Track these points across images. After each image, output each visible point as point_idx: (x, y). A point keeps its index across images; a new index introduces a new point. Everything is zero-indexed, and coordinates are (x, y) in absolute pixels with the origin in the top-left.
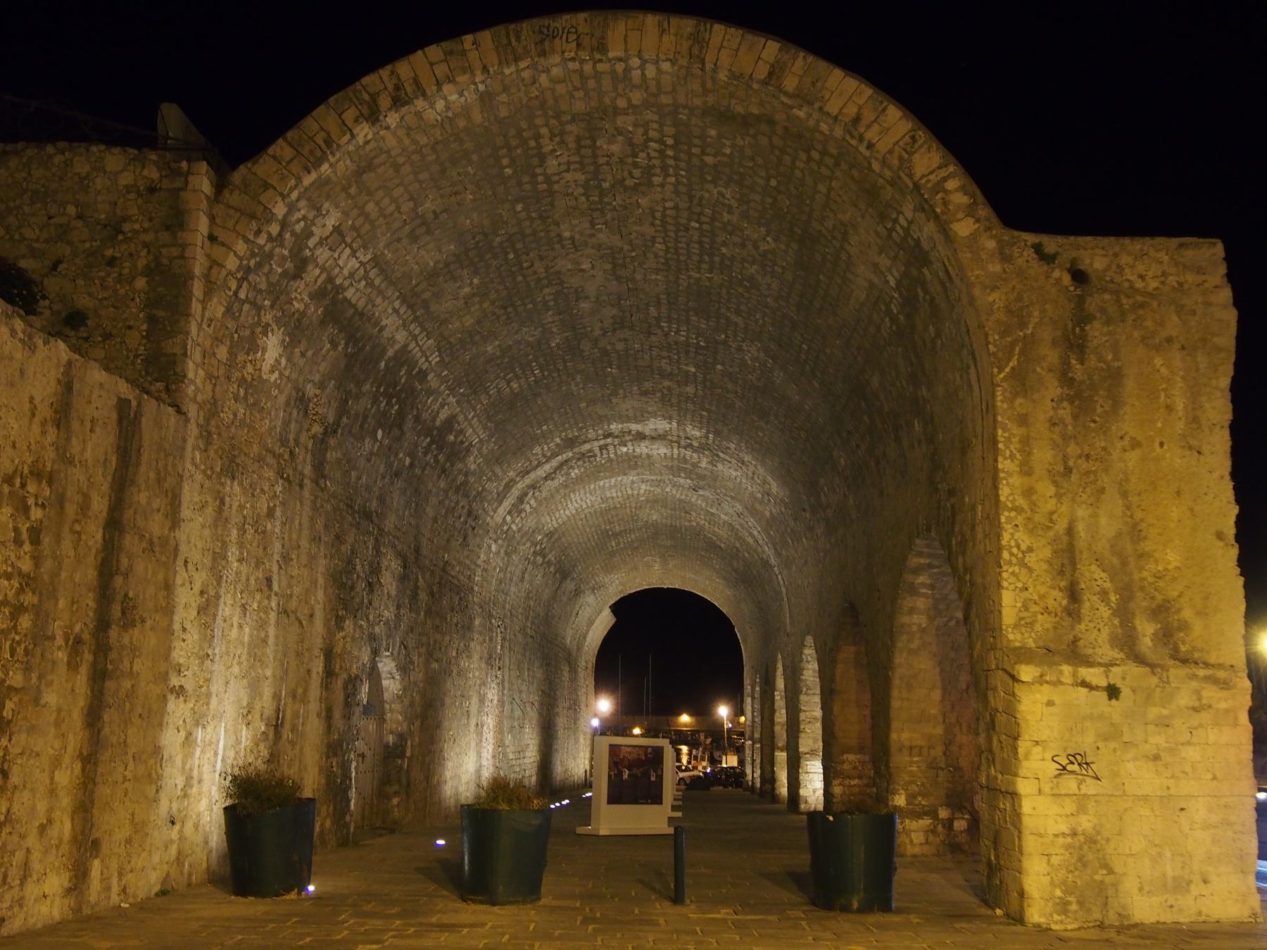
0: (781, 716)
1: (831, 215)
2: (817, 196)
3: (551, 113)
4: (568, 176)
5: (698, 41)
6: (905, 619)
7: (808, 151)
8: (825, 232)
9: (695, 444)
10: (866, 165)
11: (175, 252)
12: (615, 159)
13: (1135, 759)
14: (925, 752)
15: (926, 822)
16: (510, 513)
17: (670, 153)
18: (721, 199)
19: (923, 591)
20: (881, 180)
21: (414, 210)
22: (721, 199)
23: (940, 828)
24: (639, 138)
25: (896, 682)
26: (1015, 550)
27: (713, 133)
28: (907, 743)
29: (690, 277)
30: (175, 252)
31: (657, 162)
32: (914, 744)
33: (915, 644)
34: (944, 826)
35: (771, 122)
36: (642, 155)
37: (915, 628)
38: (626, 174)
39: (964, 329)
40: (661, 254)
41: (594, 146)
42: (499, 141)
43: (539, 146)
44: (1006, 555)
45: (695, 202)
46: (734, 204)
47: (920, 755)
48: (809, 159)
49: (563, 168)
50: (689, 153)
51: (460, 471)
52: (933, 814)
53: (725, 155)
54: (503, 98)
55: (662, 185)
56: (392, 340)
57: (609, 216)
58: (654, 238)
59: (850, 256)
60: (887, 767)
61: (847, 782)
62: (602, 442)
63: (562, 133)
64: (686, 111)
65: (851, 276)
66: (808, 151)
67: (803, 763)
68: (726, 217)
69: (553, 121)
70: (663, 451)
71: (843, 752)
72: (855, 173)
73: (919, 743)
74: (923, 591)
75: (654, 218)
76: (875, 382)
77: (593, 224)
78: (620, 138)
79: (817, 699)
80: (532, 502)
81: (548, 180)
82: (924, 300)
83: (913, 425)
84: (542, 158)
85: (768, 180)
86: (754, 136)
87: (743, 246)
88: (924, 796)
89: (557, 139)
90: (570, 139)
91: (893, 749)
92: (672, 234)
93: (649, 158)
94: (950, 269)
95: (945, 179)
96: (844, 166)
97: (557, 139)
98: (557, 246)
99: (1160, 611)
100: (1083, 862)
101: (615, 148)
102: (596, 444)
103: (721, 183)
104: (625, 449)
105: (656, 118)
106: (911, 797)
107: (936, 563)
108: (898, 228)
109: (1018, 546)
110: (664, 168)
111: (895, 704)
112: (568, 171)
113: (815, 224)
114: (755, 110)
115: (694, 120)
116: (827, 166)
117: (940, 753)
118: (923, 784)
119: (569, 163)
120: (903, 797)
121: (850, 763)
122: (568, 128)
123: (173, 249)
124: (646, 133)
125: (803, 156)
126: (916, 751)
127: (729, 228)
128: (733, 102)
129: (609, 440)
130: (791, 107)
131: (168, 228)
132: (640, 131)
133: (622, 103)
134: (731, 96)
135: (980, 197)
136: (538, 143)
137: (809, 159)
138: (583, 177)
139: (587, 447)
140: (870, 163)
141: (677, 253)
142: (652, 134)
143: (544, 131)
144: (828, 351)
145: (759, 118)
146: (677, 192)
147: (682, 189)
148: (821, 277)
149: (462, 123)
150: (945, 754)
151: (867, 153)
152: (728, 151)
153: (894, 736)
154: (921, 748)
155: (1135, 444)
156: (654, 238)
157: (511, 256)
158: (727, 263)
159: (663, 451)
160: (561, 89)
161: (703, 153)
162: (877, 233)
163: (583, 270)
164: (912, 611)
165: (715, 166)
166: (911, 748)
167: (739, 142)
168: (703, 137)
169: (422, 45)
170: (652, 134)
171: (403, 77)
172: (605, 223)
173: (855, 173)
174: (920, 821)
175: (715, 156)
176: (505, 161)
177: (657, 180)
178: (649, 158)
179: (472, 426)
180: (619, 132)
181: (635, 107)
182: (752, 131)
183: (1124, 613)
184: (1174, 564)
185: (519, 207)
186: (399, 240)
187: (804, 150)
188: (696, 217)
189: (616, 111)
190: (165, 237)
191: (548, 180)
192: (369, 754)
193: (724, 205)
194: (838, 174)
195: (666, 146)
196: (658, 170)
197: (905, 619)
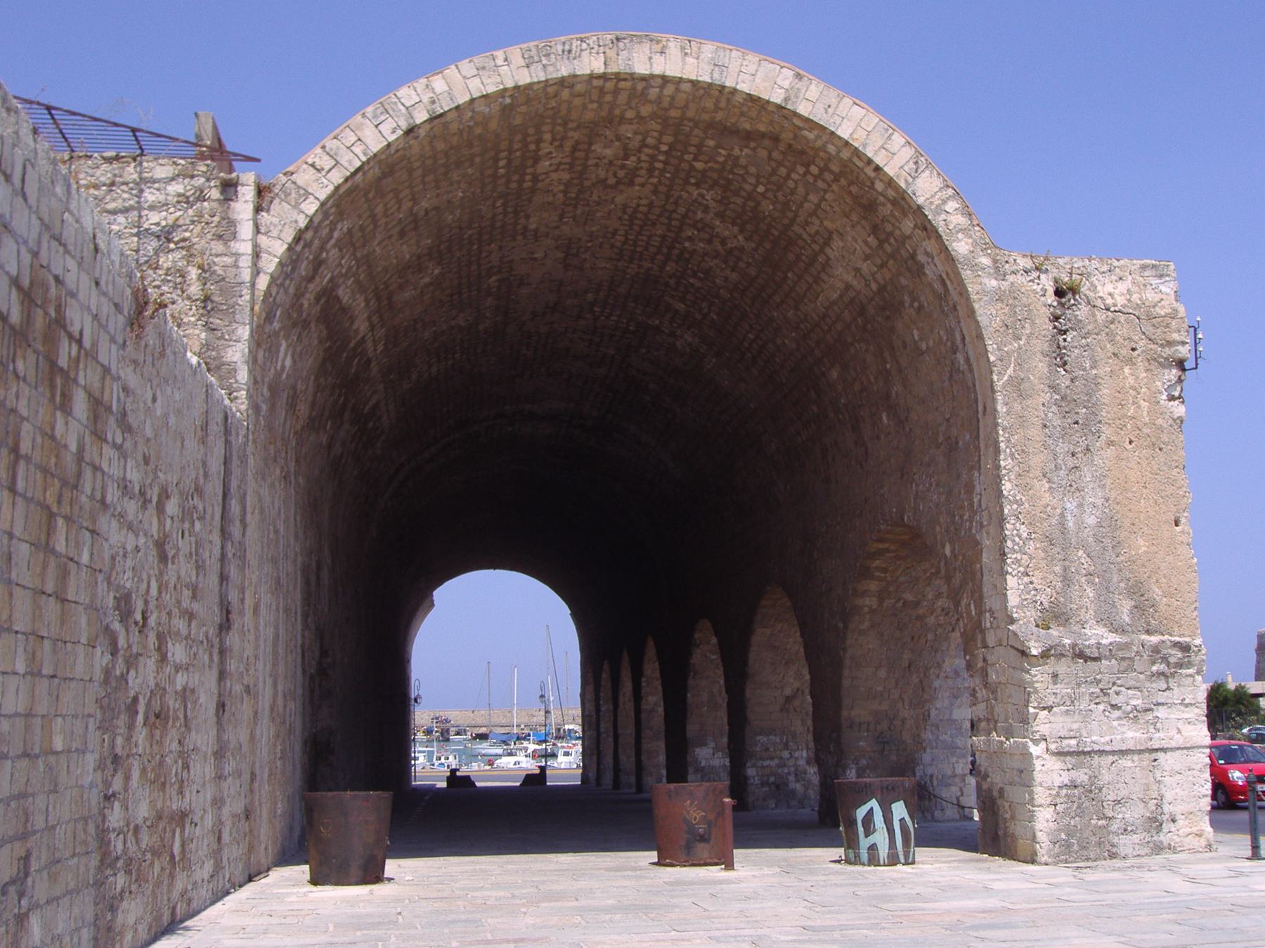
0: (605, 725)
1: (817, 222)
2: (806, 205)
3: (559, 121)
4: (554, 176)
5: (786, 99)
6: (859, 602)
7: (807, 165)
8: (805, 236)
10: (868, 184)
11: (228, 260)
12: (606, 161)
13: (1119, 718)
17: (661, 158)
18: (700, 199)
19: (877, 574)
20: (881, 198)
21: (411, 209)
22: (700, 199)
24: (635, 143)
25: (847, 662)
26: (1017, 539)
27: (711, 143)
29: (640, 267)
30: (228, 260)
31: (644, 165)
33: (866, 625)
35: (776, 139)
36: (633, 158)
37: (866, 609)
38: (610, 174)
39: (958, 337)
40: (618, 244)
41: (588, 151)
42: (504, 145)
43: (538, 149)
44: (1009, 543)
45: (671, 200)
46: (712, 204)
47: (868, 730)
48: (807, 172)
49: (553, 168)
50: (681, 159)
53: (717, 162)
54: (523, 109)
55: (642, 185)
56: (357, 331)
57: (579, 212)
58: (616, 230)
59: (829, 259)
61: (760, 763)
63: (564, 138)
64: (691, 124)
65: (825, 277)
66: (807, 165)
68: (700, 215)
69: (558, 128)
71: (760, 734)
72: (854, 189)
74: (877, 574)
75: (624, 212)
76: (834, 374)
77: (561, 217)
78: (617, 143)
81: (535, 178)
82: (911, 306)
83: (881, 419)
84: (536, 160)
85: (756, 186)
86: (754, 149)
87: (710, 241)
89: (557, 143)
90: (568, 145)
92: (637, 228)
93: (639, 160)
94: (948, 283)
95: (944, 202)
96: (843, 182)
97: (557, 143)
98: (520, 237)
99: (1136, 591)
100: (1081, 812)
101: (608, 152)
103: (706, 186)
105: (659, 127)
107: (893, 547)
108: (892, 240)
109: (1020, 537)
110: (651, 171)
111: (846, 683)
112: (556, 171)
113: (796, 228)
114: (762, 128)
115: (696, 131)
116: (824, 181)
119: (560, 163)
122: (571, 134)
123: (225, 259)
124: (643, 140)
125: (801, 170)
127: (700, 225)
128: (743, 119)
130: (800, 128)
131: (220, 237)
132: (639, 137)
133: (630, 114)
134: (742, 114)
136: (537, 146)
137: (807, 172)
138: (568, 177)
140: (873, 183)
141: (635, 245)
142: (650, 141)
143: (548, 137)
144: (779, 341)
145: (763, 135)
146: (655, 192)
147: (662, 189)
148: (789, 275)
149: (478, 131)
151: (872, 174)
152: (721, 159)
153: (845, 713)
155: (1110, 443)
156: (616, 230)
157: (475, 247)
158: (686, 255)
160: (577, 101)
161: (695, 159)
162: (866, 242)
163: (535, 259)
164: (864, 593)
165: (704, 171)
167: (737, 152)
168: (700, 146)
169: (455, 60)
170: (650, 141)
171: (438, 90)
172: (574, 218)
173: (854, 189)
175: (706, 163)
176: (502, 163)
177: (638, 180)
178: (639, 160)
180: (618, 138)
181: (642, 118)
182: (753, 144)
183: (1105, 591)
184: (1144, 549)
185: (499, 204)
186: (390, 237)
187: (802, 165)
188: (667, 214)
189: (622, 119)
190: (218, 247)
191: (535, 178)
193: (700, 204)
194: (835, 187)
195: (660, 152)
196: (643, 172)
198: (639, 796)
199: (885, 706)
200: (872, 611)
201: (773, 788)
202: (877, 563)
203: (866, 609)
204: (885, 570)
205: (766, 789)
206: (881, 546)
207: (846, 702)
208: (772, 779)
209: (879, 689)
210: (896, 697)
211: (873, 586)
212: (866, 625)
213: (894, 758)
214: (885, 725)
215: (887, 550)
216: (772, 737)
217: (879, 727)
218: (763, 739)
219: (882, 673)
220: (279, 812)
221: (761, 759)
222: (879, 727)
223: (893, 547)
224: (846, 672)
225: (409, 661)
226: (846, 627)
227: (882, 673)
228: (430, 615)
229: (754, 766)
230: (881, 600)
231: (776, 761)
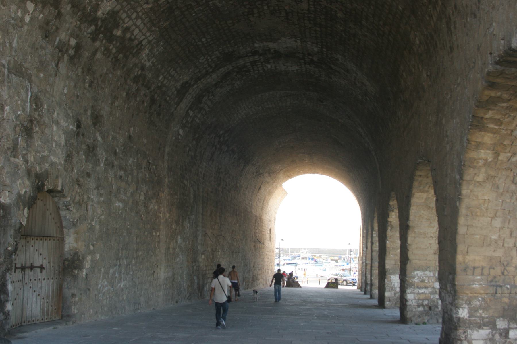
9: (315, 59)
14: (486, 272)
15: (485, 332)
16: (191, 108)
19: (492, 126)
23: (497, 337)
25: (463, 211)
28: (471, 264)
32: (476, 265)
34: (501, 335)
37: (481, 163)
47: (482, 274)
51: (135, 65)
52: (492, 324)
60: (454, 285)
61: (417, 291)
62: (251, 59)
67: (388, 276)
70: (295, 68)
71: (415, 270)
73: (484, 264)
74: (492, 126)
79: (398, 234)
80: (209, 103)
88: (485, 309)
91: (459, 268)
102: (247, 60)
104: (269, 66)
106: (472, 311)
107: (506, 96)
111: (462, 230)
117: (499, 273)
118: (483, 299)
120: (466, 311)
121: (419, 278)
126: (478, 271)
129: (256, 58)
135: (406, 294)
139: (241, 62)
150: (503, 273)
153: (459, 258)
154: (483, 268)
159: (295, 68)
164: (479, 146)
166: (474, 268)
174: (481, 331)
179: (137, 27)
192: (45, 264)
197: (473, 154)
198: (380, 311)
199: (500, 253)
200: (486, 164)
201: (427, 308)
202: (489, 114)
203: (481, 163)
204: (499, 122)
205: (421, 309)
206: (493, 94)
207: (461, 248)
208: (426, 302)
209: (494, 237)
210: (511, 245)
211: (488, 139)
212: (480, 178)
213: (506, 300)
214: (498, 270)
215: (500, 99)
216: (427, 273)
217: (492, 272)
218: (419, 273)
219: (497, 223)
220: (185, 278)
221: (418, 287)
222: (492, 272)
223: (506, 96)
224: (462, 221)
225: (362, 219)
226: (461, 178)
227: (497, 223)
228: (312, 175)
229: (411, 293)
230: (497, 154)
231: (430, 290)
